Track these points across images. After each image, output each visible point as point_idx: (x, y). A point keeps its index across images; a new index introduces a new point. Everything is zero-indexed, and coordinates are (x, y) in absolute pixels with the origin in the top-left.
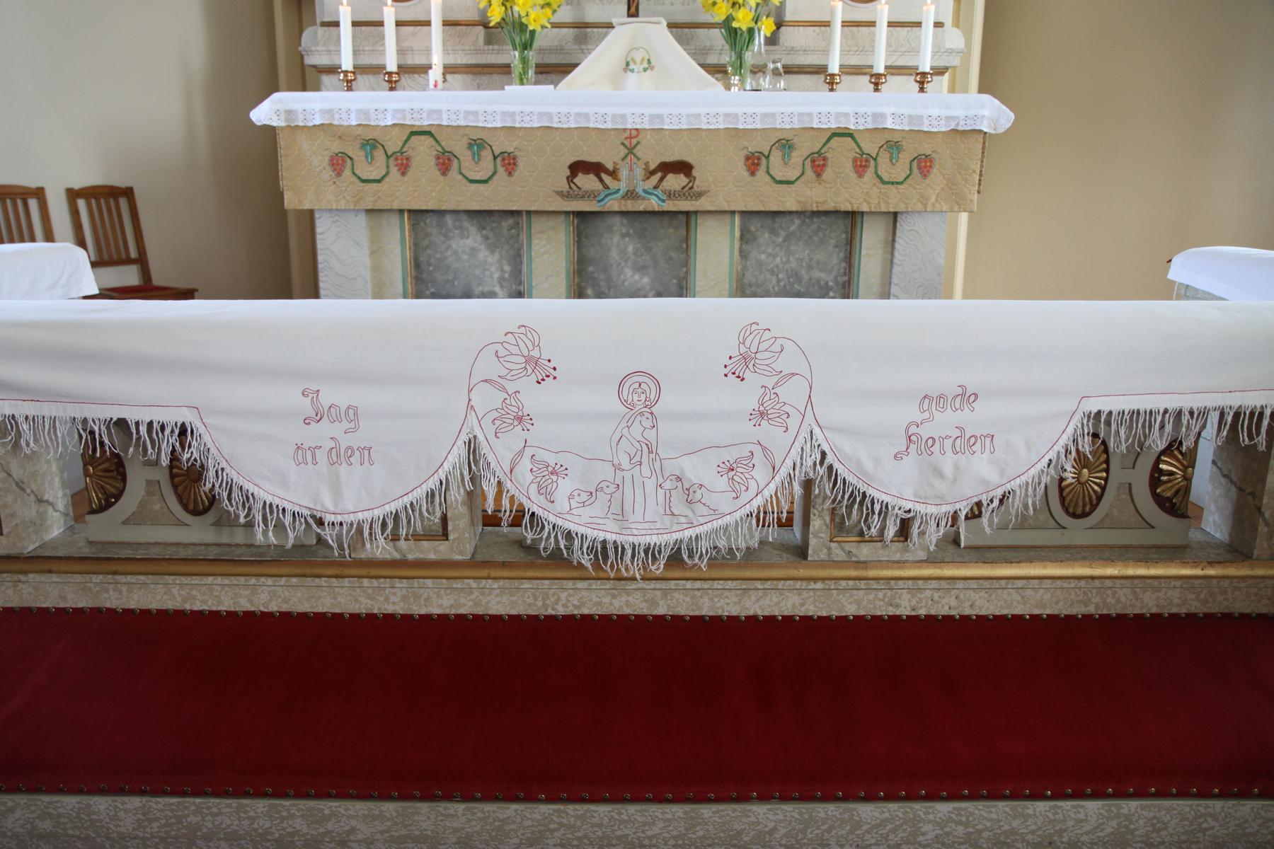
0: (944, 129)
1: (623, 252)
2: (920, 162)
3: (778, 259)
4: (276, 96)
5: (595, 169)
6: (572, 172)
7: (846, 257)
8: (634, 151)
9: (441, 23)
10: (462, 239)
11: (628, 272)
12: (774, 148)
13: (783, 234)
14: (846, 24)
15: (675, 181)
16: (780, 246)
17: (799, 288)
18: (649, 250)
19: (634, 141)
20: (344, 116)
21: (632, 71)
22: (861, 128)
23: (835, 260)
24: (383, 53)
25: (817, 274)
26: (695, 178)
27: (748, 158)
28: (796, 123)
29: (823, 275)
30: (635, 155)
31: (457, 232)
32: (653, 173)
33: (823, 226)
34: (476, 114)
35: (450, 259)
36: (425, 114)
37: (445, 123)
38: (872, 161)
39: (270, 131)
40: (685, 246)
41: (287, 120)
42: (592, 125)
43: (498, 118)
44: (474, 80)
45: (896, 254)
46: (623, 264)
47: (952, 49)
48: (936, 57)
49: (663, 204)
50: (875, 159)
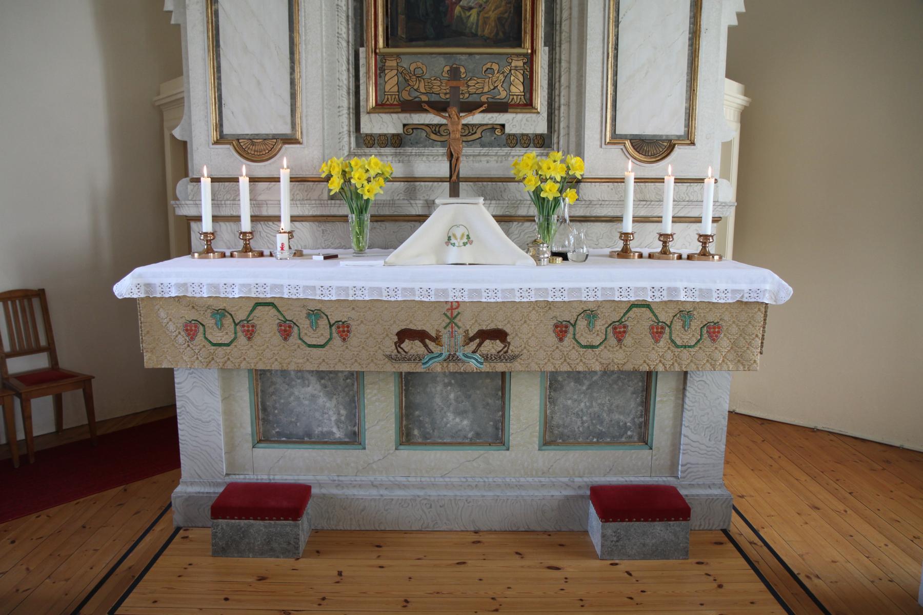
0: (730, 301)
2: (709, 328)
3: (582, 405)
4: (138, 270)
5: (421, 336)
6: (399, 339)
7: (642, 402)
8: (455, 321)
9: (289, 180)
10: (303, 387)
11: (450, 416)
12: (579, 318)
13: (587, 383)
14: (638, 180)
15: (491, 347)
16: (585, 393)
17: (601, 428)
20: (197, 289)
21: (454, 245)
22: (657, 300)
23: (632, 404)
25: (616, 416)
26: (509, 343)
27: (556, 326)
28: (600, 296)
29: (622, 417)
30: (456, 325)
31: (299, 381)
32: (472, 339)
35: (293, 404)
38: (667, 328)
39: (131, 304)
40: (500, 393)
41: (147, 292)
42: (417, 299)
43: (333, 292)
45: (687, 400)
46: (445, 409)
47: (725, 203)
49: (482, 366)
50: (669, 327)
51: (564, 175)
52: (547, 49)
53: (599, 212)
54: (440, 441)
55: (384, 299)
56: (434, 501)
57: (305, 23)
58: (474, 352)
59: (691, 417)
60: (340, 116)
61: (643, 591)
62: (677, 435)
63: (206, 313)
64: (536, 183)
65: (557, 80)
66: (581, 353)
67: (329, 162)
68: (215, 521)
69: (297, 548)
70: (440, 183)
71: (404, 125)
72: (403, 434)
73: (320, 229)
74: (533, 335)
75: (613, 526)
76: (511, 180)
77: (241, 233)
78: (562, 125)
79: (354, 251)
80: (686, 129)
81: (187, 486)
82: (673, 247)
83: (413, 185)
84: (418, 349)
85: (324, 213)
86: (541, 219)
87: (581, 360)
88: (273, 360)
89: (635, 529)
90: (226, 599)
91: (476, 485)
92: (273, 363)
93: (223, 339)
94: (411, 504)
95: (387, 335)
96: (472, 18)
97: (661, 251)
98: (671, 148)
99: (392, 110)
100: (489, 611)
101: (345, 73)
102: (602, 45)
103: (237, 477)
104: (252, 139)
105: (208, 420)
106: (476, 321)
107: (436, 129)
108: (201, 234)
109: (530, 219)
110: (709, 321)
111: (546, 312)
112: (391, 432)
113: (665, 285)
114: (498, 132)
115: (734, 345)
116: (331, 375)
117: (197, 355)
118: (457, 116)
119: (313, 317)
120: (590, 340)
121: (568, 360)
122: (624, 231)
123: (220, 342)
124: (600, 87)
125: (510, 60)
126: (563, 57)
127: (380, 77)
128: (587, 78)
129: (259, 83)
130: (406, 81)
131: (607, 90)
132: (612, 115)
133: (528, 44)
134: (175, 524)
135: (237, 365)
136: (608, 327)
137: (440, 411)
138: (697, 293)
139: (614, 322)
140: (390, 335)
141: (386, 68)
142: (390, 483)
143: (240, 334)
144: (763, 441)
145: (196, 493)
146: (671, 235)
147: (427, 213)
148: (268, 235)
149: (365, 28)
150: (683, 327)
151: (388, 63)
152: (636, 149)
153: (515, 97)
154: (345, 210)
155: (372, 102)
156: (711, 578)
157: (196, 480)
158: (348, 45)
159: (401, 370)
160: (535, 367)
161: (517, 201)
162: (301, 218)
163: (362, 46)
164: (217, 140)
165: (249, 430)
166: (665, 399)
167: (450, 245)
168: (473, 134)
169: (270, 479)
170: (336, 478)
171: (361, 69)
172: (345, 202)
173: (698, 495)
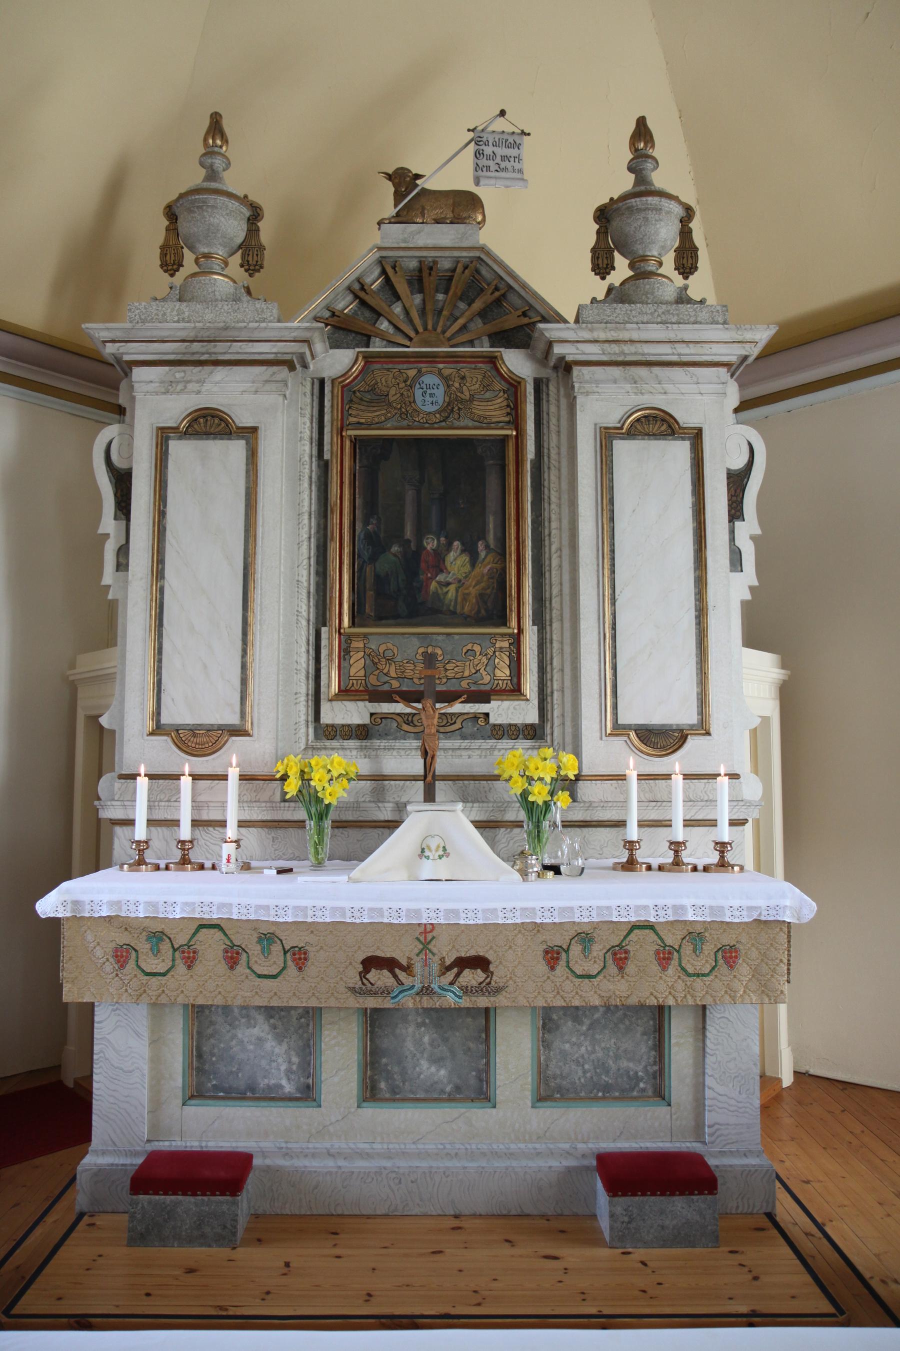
0: (746, 920)
1: (418, 1043)
2: (724, 952)
3: (583, 1049)
4: (65, 885)
5: (390, 964)
6: (364, 968)
7: (655, 1045)
8: (430, 947)
10: (248, 1028)
11: (424, 1064)
12: (573, 942)
13: (587, 1022)
14: (641, 777)
15: (472, 977)
17: (607, 1079)
18: (445, 1040)
19: (429, 936)
20: (132, 908)
21: (428, 858)
22: (662, 920)
23: (643, 1049)
24: (178, 808)
25: (624, 1064)
26: (492, 973)
27: (546, 952)
29: (631, 1065)
30: (430, 951)
31: (243, 1020)
32: (449, 968)
33: (629, 1013)
34: (267, 908)
35: (235, 1049)
36: (215, 907)
37: (235, 917)
38: (675, 953)
39: (55, 923)
40: (484, 1036)
41: (73, 910)
42: (386, 920)
43: (290, 912)
44: (269, 834)
45: (708, 1042)
46: (418, 1055)
48: (735, 810)
50: (678, 951)
51: (555, 776)
52: (535, 628)
53: (601, 815)
54: (412, 1096)
55: (348, 920)
56: (404, 1174)
57: (261, 602)
58: (451, 983)
59: (715, 1063)
60: (296, 703)
61: (659, 1284)
62: (700, 1087)
63: (141, 936)
64: (523, 786)
65: (549, 662)
66: (577, 984)
67: (286, 761)
68: (135, 1197)
69: (234, 1234)
70: (413, 782)
71: (372, 714)
72: (367, 1087)
73: (270, 837)
74: (520, 963)
75: (623, 1201)
76: (497, 778)
77: (179, 842)
78: (556, 713)
79: (311, 864)
80: (700, 717)
81: (98, 1155)
82: (687, 857)
83: (382, 784)
84: (387, 980)
85: (276, 818)
86: (530, 825)
87: (577, 993)
88: (216, 993)
89: (650, 1206)
90: (148, 1295)
91: (456, 1154)
92: (216, 997)
93: (159, 967)
94: (375, 1178)
95: (351, 963)
96: (450, 595)
97: (673, 863)
98: (683, 739)
99: (357, 698)
100: (470, 1305)
101: (304, 655)
102: (597, 625)
103: (161, 1143)
104: (193, 730)
105: (131, 1069)
106: (454, 947)
107: (408, 719)
108: (133, 843)
109: (518, 824)
110: (723, 944)
111: (534, 935)
112: (352, 1084)
113: (670, 902)
114: (481, 722)
115: (756, 973)
116: (283, 1013)
117: (126, 986)
118: (433, 709)
119: (265, 942)
120: (586, 969)
121: (562, 993)
122: (629, 839)
123: (155, 971)
124: (597, 671)
125: (494, 641)
126: (555, 637)
127: (345, 659)
128: (582, 661)
129: (205, 667)
130: (375, 664)
131: (605, 674)
132: (613, 702)
133: (514, 623)
134: (77, 1209)
135: (173, 999)
136: (606, 953)
137: (413, 1059)
138: (707, 911)
139: (613, 947)
140: (354, 964)
141: (351, 649)
142: (350, 1151)
143: (179, 961)
144: (843, 1111)
145: (108, 1165)
146: (683, 843)
147: (397, 818)
148: (207, 843)
149: (328, 607)
150: (694, 951)
151: (355, 644)
152: (642, 741)
153: (500, 682)
154: (302, 814)
155: (334, 688)
156: (746, 1269)
157: (110, 1148)
158: (309, 624)
159: (366, 1006)
160: (523, 1002)
161: (504, 803)
162: (248, 824)
163: (325, 625)
164: (153, 730)
165: (179, 1082)
166: (682, 1041)
167: (424, 858)
168: (452, 724)
169: (202, 1147)
170: (283, 1145)
171: (322, 651)
172: (301, 805)
173: (731, 1166)
